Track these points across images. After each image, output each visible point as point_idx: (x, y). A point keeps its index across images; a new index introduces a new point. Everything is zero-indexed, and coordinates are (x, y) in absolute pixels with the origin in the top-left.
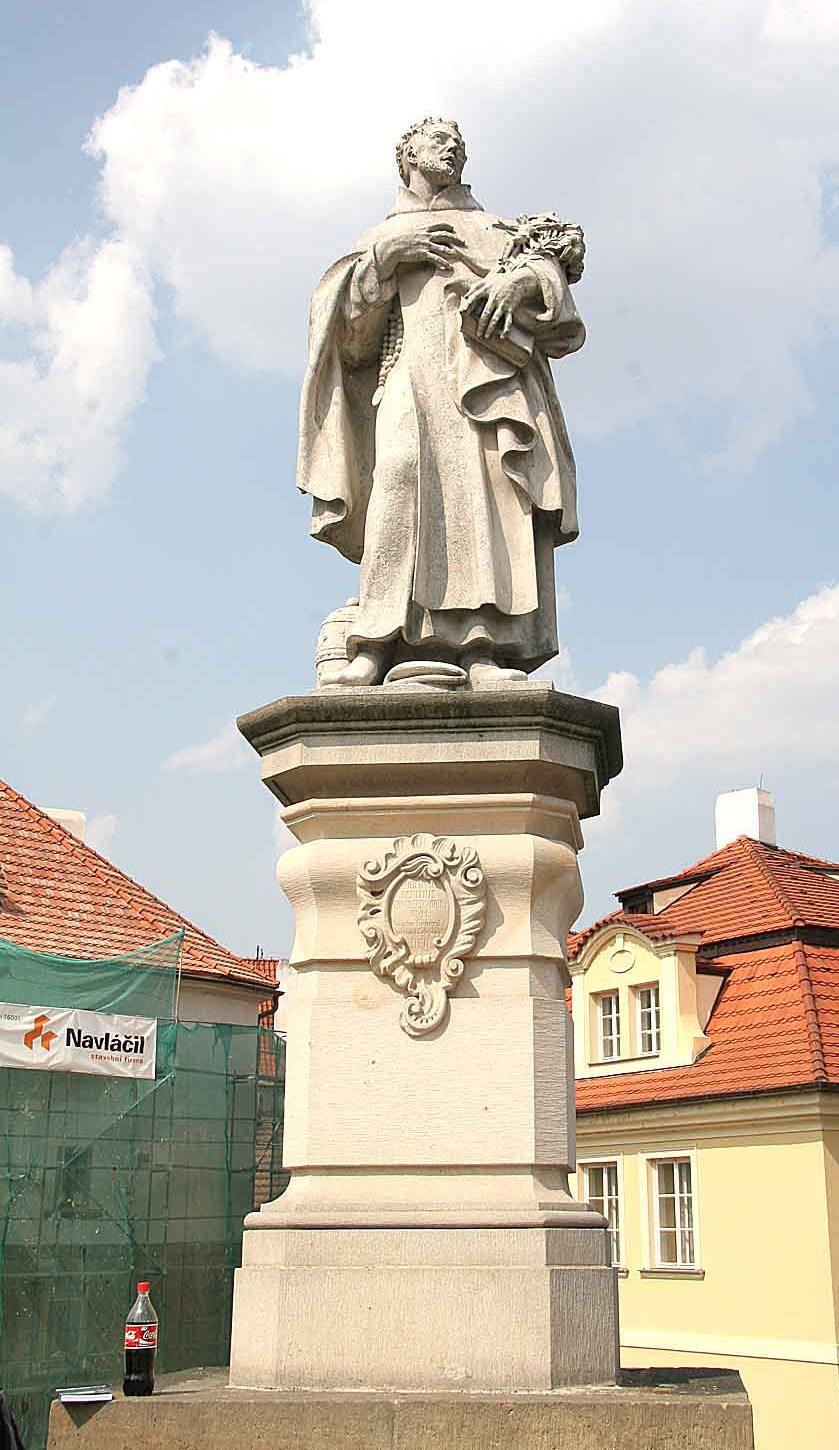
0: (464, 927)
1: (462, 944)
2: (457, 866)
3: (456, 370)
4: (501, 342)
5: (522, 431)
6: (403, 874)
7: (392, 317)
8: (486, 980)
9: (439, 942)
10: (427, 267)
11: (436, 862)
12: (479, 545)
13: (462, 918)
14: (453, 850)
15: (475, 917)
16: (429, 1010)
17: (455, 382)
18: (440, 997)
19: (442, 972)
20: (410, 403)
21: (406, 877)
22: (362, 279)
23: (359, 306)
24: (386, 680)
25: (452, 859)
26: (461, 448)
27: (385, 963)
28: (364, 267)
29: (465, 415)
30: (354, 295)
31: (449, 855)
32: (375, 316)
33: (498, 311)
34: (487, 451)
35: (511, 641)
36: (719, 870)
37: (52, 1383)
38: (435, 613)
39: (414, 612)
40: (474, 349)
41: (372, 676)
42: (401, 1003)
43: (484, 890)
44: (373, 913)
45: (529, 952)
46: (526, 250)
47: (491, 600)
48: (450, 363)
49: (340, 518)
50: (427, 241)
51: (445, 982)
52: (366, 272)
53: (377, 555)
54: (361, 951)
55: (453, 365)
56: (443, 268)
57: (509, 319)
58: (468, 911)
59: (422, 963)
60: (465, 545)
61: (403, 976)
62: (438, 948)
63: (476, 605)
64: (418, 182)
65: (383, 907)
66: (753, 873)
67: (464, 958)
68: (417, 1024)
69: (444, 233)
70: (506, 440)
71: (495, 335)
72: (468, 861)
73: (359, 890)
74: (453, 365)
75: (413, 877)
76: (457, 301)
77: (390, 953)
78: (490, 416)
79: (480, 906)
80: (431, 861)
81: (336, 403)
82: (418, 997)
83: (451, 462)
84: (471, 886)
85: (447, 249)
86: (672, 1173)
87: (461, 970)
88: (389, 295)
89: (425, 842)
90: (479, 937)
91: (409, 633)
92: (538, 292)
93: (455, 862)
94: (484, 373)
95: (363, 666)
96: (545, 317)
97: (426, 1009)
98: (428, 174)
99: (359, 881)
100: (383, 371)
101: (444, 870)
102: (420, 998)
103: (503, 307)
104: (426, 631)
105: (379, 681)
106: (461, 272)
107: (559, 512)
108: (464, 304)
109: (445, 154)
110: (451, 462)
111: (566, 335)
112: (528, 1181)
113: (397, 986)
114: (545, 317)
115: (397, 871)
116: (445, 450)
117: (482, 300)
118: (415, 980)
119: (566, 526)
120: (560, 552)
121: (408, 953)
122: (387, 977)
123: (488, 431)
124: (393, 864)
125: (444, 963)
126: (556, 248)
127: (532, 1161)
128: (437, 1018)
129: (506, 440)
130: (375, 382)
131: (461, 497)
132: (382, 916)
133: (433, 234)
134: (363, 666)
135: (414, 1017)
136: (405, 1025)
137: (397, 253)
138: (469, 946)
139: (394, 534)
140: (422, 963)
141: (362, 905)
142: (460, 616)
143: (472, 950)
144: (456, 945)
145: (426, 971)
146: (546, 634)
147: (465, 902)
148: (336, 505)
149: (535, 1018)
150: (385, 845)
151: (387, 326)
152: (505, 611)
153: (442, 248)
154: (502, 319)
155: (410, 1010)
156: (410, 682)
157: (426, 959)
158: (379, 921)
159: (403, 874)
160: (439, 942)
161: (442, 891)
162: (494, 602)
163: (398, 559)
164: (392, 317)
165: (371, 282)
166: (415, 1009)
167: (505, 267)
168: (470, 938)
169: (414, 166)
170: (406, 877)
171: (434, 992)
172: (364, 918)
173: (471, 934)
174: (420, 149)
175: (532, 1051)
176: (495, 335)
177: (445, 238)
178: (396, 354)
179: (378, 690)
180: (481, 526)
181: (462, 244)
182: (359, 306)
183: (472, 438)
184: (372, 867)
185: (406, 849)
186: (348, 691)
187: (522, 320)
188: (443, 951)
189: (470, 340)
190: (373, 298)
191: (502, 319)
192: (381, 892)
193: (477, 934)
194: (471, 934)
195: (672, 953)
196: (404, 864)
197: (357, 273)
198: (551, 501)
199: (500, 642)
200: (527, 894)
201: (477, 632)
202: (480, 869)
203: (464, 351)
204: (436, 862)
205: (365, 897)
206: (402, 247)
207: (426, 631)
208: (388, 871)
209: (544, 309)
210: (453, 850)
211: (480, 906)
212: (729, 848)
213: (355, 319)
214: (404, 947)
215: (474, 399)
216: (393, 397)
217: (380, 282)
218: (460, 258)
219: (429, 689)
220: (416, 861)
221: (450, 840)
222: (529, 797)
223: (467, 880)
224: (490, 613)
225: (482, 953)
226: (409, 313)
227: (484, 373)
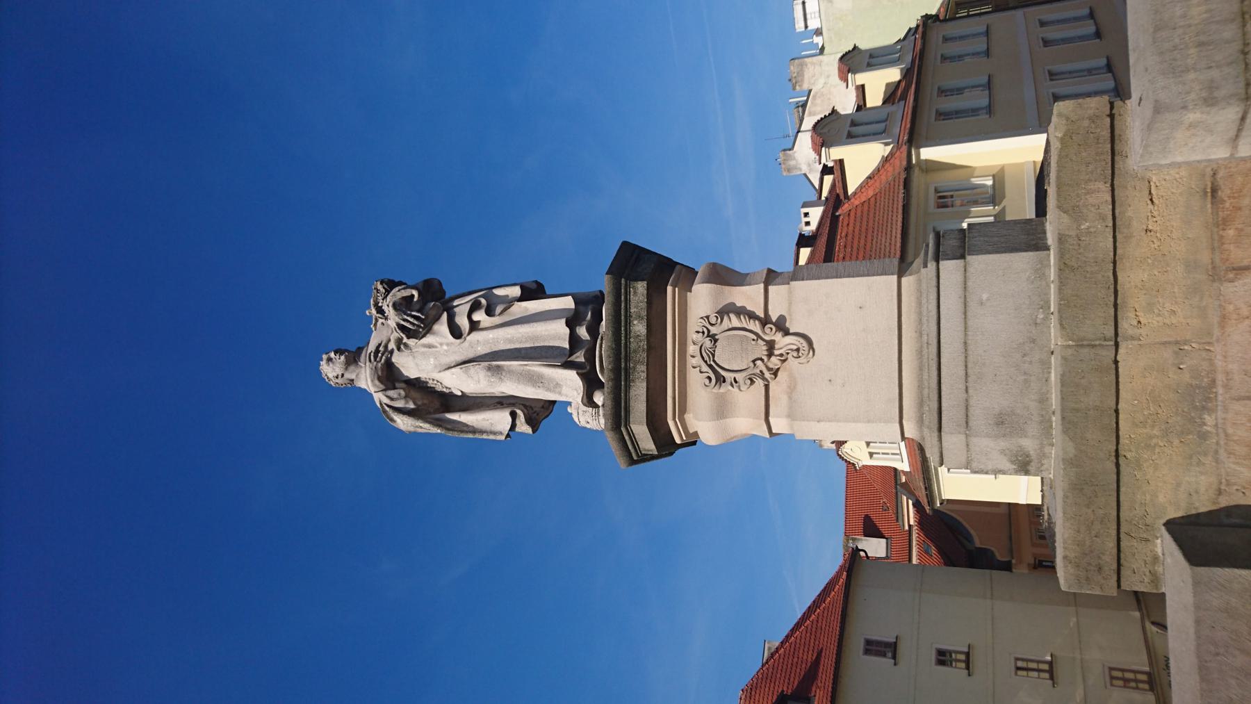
0: (745, 325)
1: (755, 326)
5: (475, 306)
9: (754, 340)
14: (698, 332)
17: (448, 345)
18: (789, 339)
20: (457, 370)
21: (714, 361)
22: (392, 399)
23: (407, 402)
25: (703, 333)
26: (480, 342)
27: (767, 375)
28: (385, 397)
31: (701, 334)
32: (413, 393)
37: (369, 308)
39: (568, 365)
42: (792, 362)
43: (723, 312)
44: (736, 382)
45: (762, 285)
47: (563, 321)
48: (436, 347)
52: (387, 396)
55: (438, 345)
59: (767, 350)
60: (536, 338)
62: (757, 340)
63: (567, 331)
65: (732, 375)
70: (479, 316)
74: (438, 345)
75: (713, 356)
76: (406, 345)
77: (761, 371)
84: (719, 319)
86: (942, 92)
88: (403, 385)
89: (692, 349)
90: (752, 316)
91: (582, 369)
94: (442, 327)
99: (715, 390)
102: (789, 351)
107: (522, 287)
108: (405, 340)
109: (338, 356)
112: (904, 280)
115: (710, 366)
116: (481, 350)
117: (402, 328)
119: (534, 286)
123: (474, 326)
124: (705, 368)
125: (767, 338)
127: (895, 277)
128: (802, 340)
130: (452, 395)
131: (510, 341)
132: (738, 376)
134: (599, 398)
137: (379, 379)
138: (757, 322)
140: (767, 350)
142: (574, 340)
145: (771, 346)
151: (417, 386)
152: (572, 313)
153: (380, 355)
155: (797, 358)
157: (765, 348)
160: (754, 340)
162: (565, 319)
165: (392, 393)
169: (343, 375)
170: (714, 361)
171: (783, 342)
172: (739, 388)
178: (435, 382)
181: (380, 345)
182: (407, 402)
183: (476, 336)
184: (707, 381)
185: (697, 361)
187: (417, 307)
190: (403, 393)
196: (706, 362)
198: (516, 291)
200: (727, 288)
201: (582, 332)
203: (428, 339)
206: (376, 375)
208: (710, 371)
209: (413, 296)
210: (698, 332)
213: (415, 404)
215: (456, 332)
216: (457, 382)
217: (394, 388)
220: (704, 354)
222: (669, 289)
224: (572, 323)
225: (762, 315)
227: (442, 327)
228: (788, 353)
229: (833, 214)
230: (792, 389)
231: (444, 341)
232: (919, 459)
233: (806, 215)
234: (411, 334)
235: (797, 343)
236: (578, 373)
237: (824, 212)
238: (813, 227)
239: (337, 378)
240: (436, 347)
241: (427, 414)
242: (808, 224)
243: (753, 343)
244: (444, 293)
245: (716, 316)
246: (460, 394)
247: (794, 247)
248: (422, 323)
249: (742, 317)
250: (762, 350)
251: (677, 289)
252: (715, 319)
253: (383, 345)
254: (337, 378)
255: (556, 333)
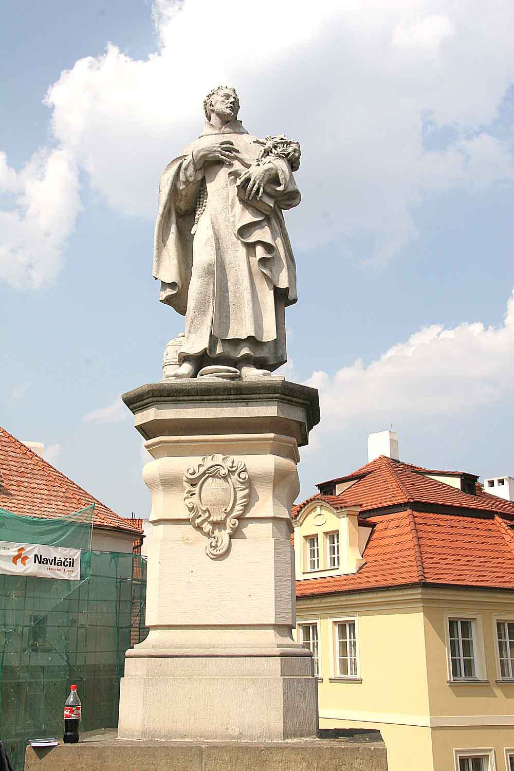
0: (238, 502)
1: (238, 511)
2: (235, 471)
3: (234, 216)
4: (258, 201)
5: (269, 247)
6: (207, 475)
7: (201, 188)
8: (250, 529)
9: (226, 510)
10: (219, 163)
11: (224, 469)
12: (246, 306)
13: (238, 498)
14: (233, 462)
15: (244, 497)
16: (221, 545)
19: (227, 525)
20: (211, 233)
21: (209, 476)
22: (186, 169)
23: (184, 183)
24: (198, 375)
25: (232, 467)
26: (237, 256)
27: (198, 521)
29: (239, 239)
30: (182, 177)
31: (231, 465)
32: (193, 188)
33: (256, 186)
34: (250, 258)
35: (263, 355)
36: (370, 473)
38: (224, 341)
39: (213, 340)
40: (243, 205)
41: (191, 373)
42: (206, 541)
43: (249, 483)
44: (191, 495)
46: (270, 154)
47: (253, 334)
48: (232, 212)
49: (175, 292)
50: (219, 149)
51: (229, 531)
52: (188, 165)
53: (194, 311)
54: (186, 514)
56: (228, 163)
57: (261, 190)
58: (240, 494)
59: (217, 521)
60: (239, 306)
61: (207, 527)
62: (225, 513)
63: (244, 337)
64: (215, 119)
65: (197, 492)
66: (387, 475)
67: (239, 518)
68: (214, 552)
69: (228, 145)
70: (260, 252)
71: (255, 198)
72: (241, 468)
73: (184, 483)
74: (233, 214)
75: (212, 477)
76: (235, 181)
77: (200, 516)
78: (252, 239)
79: (247, 491)
80: (222, 468)
81: (173, 233)
82: (215, 538)
83: (232, 263)
84: (242, 481)
85: (230, 153)
87: (237, 525)
88: (200, 177)
89: (219, 459)
90: (246, 507)
92: (277, 176)
93: (234, 469)
95: (187, 368)
96: (280, 188)
97: (219, 544)
98: (220, 115)
99: (185, 478)
100: (197, 217)
101: (228, 473)
102: (216, 539)
103: (259, 184)
104: (219, 350)
105: (195, 376)
106: (237, 166)
107: (287, 289)
108: (239, 182)
109: (229, 105)
110: (232, 263)
111: (291, 198)
112: (271, 633)
113: (204, 532)
114: (280, 188)
115: (204, 473)
116: (228, 257)
117: (248, 180)
118: (214, 529)
119: (291, 296)
120: (288, 310)
121: (210, 516)
122: (199, 528)
123: (251, 247)
124: (202, 470)
125: (228, 520)
126: (286, 153)
129: (260, 252)
130: (193, 222)
132: (196, 496)
133: (222, 146)
134: (187, 368)
135: (213, 548)
136: (209, 552)
138: (241, 512)
139: (202, 300)
140: (217, 521)
141: (186, 491)
142: (236, 343)
143: (243, 514)
144: (234, 511)
146: (280, 352)
147: (239, 489)
148: (173, 285)
149: (275, 549)
150: (198, 460)
151: (199, 194)
152: (260, 340)
153: (227, 153)
154: (258, 189)
155: (211, 545)
156: (211, 376)
158: (195, 499)
159: (207, 475)
160: (226, 510)
161: (227, 484)
163: (204, 313)
164: (201, 188)
166: (213, 544)
167: (260, 163)
168: (242, 508)
170: (209, 476)
173: (242, 506)
174: (216, 103)
175: (273, 566)
176: (255, 198)
177: (229, 148)
178: (204, 208)
179: (194, 380)
180: (247, 296)
181: (237, 151)
182: (184, 183)
183: (243, 251)
185: (209, 462)
186: (179, 381)
187: (269, 190)
188: (228, 514)
189: (242, 201)
190: (192, 179)
191: (258, 189)
192: (196, 484)
193: (245, 506)
194: (242, 506)
195: (346, 515)
196: (208, 470)
197: (184, 166)
198: (283, 283)
199: (257, 356)
200: (271, 485)
202: (247, 472)
203: (239, 206)
204: (224, 469)
205: (188, 487)
206: (206, 152)
207: (219, 350)
208: (200, 474)
209: (280, 185)
210: (233, 462)
211: (247, 491)
212: (375, 462)
214: (208, 512)
215: (244, 231)
216: (202, 230)
217: (196, 170)
218: (236, 158)
219: (220, 380)
220: (214, 469)
221: (231, 458)
222: (272, 435)
223: (240, 478)
225: (248, 515)
226: (210, 187)
228: (215, 538)
229: (497, 513)
230: (186, 541)
231: (237, 219)
232: (166, 628)
233: (502, 482)
234: (243, 187)
235: (223, 545)
236: (206, 348)
237: (504, 502)
238: (487, 489)
239: (211, 105)
240: (232, 212)
241: (175, 200)
242: (491, 483)
243: (223, 509)
244: (288, 207)
245: (245, 478)
246: (193, 232)
247: (461, 470)
248: (252, 198)
249: (245, 500)
250: (216, 518)
251: (272, 442)
252: (244, 477)
253: (237, 154)
254: (211, 105)
255: (241, 328)
